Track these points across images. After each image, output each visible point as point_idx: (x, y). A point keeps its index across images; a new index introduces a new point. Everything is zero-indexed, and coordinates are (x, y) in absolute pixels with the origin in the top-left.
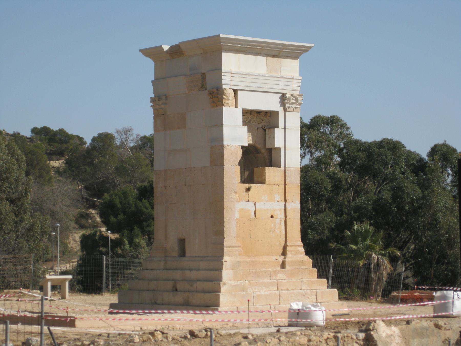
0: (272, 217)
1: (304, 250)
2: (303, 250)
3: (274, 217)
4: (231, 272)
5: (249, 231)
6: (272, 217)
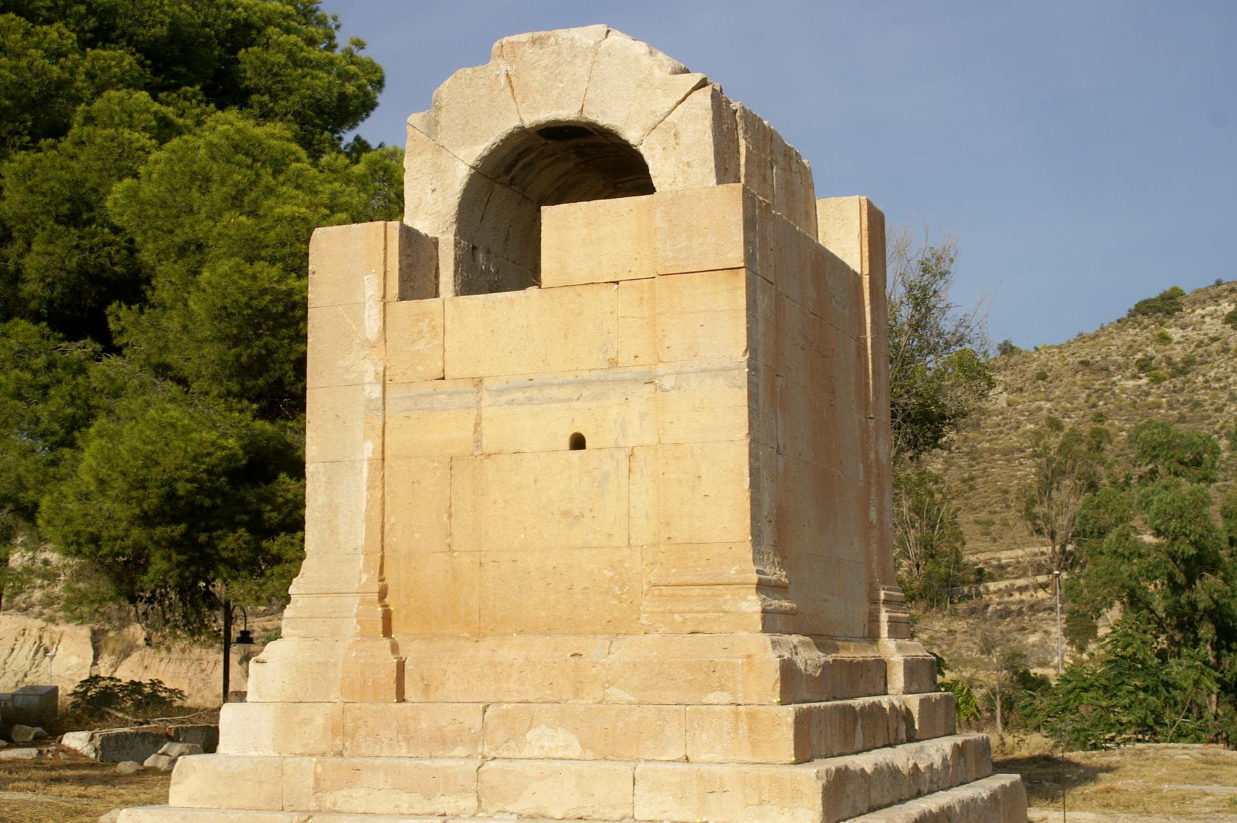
5: (445, 516)
6: (578, 442)
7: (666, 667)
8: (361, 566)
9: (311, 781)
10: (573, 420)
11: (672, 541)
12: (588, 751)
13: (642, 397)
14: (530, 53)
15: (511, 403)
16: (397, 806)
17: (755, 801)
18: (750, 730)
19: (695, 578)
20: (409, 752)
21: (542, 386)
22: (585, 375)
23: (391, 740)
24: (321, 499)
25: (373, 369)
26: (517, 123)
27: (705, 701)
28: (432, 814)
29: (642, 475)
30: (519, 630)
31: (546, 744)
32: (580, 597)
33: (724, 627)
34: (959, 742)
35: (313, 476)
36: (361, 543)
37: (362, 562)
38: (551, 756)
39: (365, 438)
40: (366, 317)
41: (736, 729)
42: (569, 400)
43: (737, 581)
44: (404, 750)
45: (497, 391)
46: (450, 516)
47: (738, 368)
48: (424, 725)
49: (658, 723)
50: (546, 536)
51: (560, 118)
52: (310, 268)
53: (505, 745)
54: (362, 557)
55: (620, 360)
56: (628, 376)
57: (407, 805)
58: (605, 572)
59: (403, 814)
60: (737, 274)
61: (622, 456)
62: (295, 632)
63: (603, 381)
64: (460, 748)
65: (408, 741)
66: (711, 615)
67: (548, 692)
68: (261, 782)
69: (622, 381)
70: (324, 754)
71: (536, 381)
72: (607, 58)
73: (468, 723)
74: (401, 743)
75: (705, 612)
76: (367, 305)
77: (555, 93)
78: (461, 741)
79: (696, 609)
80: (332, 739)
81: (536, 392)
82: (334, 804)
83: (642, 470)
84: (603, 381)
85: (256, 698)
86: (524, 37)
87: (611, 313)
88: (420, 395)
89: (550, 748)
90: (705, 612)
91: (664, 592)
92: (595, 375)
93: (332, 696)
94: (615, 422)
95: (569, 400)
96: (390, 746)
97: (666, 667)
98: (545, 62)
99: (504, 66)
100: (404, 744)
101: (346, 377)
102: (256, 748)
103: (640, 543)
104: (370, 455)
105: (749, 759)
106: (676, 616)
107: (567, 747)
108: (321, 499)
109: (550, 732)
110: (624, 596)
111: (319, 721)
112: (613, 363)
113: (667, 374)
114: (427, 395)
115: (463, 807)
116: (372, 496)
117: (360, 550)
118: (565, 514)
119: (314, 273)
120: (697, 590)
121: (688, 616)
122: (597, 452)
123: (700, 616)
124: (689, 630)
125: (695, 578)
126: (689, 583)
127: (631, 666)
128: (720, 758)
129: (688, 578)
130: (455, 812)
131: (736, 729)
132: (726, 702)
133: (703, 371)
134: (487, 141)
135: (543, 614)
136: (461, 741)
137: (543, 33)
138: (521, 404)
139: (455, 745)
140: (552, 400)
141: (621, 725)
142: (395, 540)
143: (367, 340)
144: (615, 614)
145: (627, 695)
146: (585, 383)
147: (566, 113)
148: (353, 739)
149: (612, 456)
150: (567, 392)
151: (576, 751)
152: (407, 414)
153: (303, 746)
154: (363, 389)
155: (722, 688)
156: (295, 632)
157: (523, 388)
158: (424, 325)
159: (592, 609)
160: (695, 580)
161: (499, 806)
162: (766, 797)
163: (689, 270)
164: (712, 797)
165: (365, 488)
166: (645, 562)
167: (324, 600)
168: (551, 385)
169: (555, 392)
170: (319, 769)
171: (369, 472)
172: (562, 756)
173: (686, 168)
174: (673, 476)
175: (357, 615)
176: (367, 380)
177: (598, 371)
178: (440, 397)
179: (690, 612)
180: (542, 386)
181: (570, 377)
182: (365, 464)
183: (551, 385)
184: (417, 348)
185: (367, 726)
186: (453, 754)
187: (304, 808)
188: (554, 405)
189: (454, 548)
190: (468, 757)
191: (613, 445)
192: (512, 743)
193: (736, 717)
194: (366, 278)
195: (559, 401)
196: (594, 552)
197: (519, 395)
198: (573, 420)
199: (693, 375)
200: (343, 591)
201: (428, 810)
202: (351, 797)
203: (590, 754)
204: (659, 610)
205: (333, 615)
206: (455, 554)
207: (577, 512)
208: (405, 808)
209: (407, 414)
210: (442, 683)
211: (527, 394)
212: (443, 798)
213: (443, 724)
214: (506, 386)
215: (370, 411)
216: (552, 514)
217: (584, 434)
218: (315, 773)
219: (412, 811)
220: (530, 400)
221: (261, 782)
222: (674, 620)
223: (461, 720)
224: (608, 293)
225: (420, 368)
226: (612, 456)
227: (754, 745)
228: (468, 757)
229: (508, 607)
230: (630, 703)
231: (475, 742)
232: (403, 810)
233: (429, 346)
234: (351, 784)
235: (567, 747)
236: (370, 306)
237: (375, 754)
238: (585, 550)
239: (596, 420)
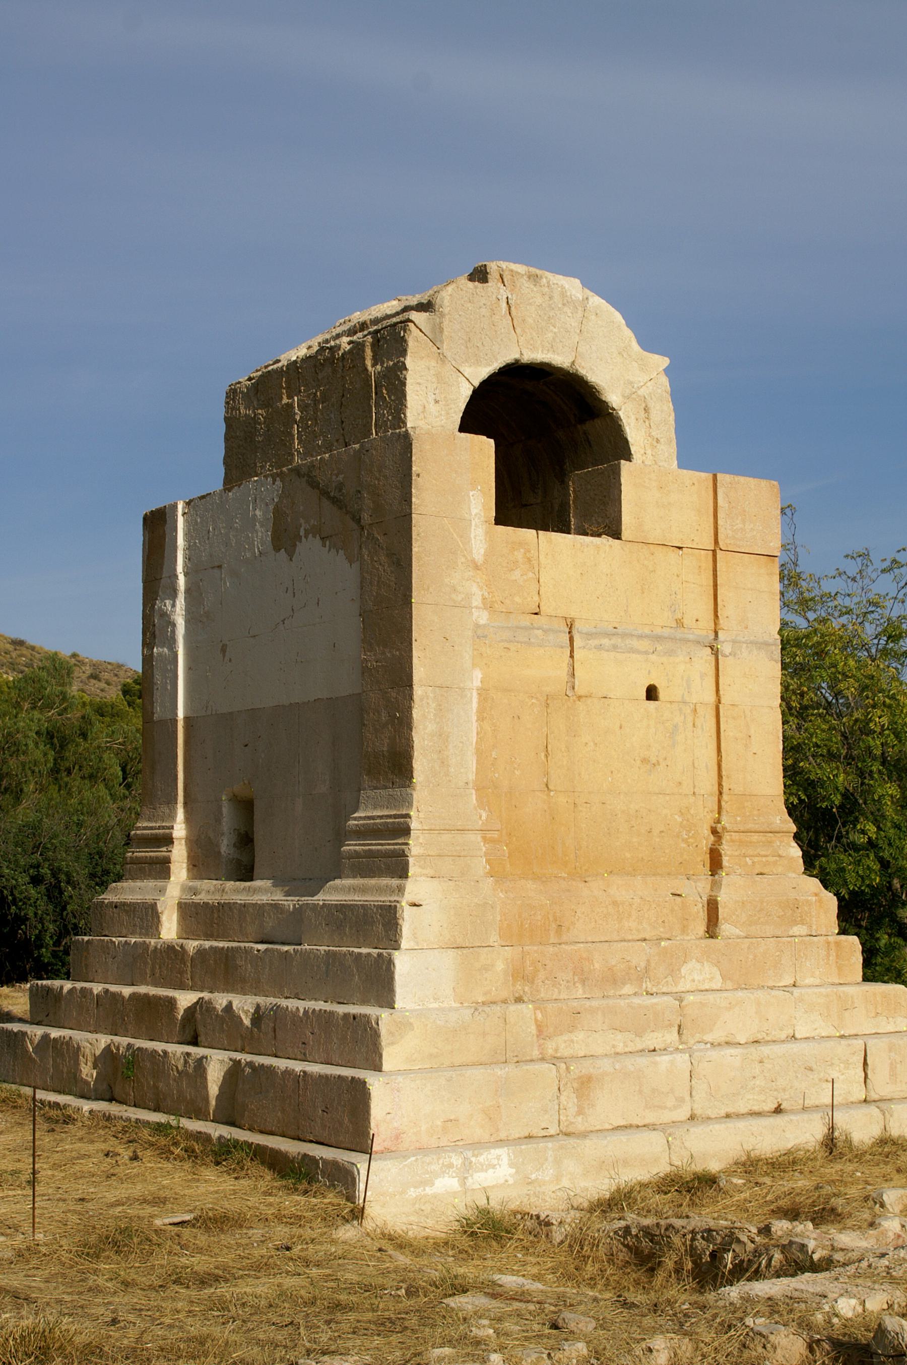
0: (652, 693)
1: (800, 853)
2: (796, 852)
3: (662, 694)
4: (447, 961)
5: (543, 755)
6: (652, 693)
7: (765, 904)
8: (475, 801)
9: (533, 1029)
10: (649, 672)
11: (732, 792)
12: (728, 982)
13: (702, 658)
14: (526, 286)
15: (599, 647)
16: (614, 1046)
17: (873, 1014)
18: (837, 956)
19: (757, 826)
20: (584, 993)
21: (624, 635)
22: (658, 631)
23: (568, 982)
24: (431, 727)
25: (480, 593)
26: (517, 356)
27: (791, 933)
28: (642, 1051)
29: (703, 729)
30: (609, 870)
31: (696, 978)
32: (658, 840)
33: (780, 869)
34: (262, 1004)
35: (422, 700)
36: (472, 777)
37: (474, 797)
38: (699, 988)
39: (474, 665)
40: (472, 536)
41: (828, 955)
42: (646, 653)
43: (785, 830)
44: (581, 991)
45: (586, 634)
46: (547, 756)
47: (775, 645)
48: (597, 966)
49: (777, 954)
50: (629, 780)
51: (554, 362)
52: (414, 469)
53: (665, 980)
54: (474, 792)
55: (685, 621)
56: (691, 637)
57: (621, 1045)
58: (676, 817)
59: (618, 1053)
60: (773, 562)
61: (688, 710)
62: (424, 871)
63: (672, 639)
64: (628, 986)
65: (583, 982)
66: (771, 859)
67: (662, 929)
68: (484, 1034)
69: (687, 641)
70: (505, 1002)
71: (619, 631)
72: (593, 317)
73: (634, 963)
74: (577, 985)
75: (767, 856)
76: (473, 523)
77: (550, 335)
78: (629, 979)
79: (763, 853)
80: (513, 985)
81: (620, 640)
82: (556, 1050)
83: (702, 725)
84: (672, 639)
85: (412, 945)
86: (520, 268)
87: (678, 576)
88: (517, 627)
89: (699, 981)
90: (767, 856)
91: (733, 837)
92: (666, 632)
93: (491, 940)
94: (682, 678)
95: (646, 653)
96: (568, 988)
97: (765, 904)
98: (539, 300)
99: (504, 293)
100: (579, 985)
101: (454, 596)
102: (436, 999)
103: (702, 792)
104: (479, 684)
105: (837, 981)
106: (748, 859)
107: (711, 979)
108: (431, 727)
109: (698, 966)
110: (691, 840)
111: (500, 966)
112: (680, 623)
113: (727, 641)
114: (525, 628)
115: (669, 1041)
116: (482, 728)
117: (471, 785)
118: (645, 761)
119: (418, 475)
120: (755, 837)
121: (756, 859)
122: (669, 705)
123: (764, 859)
124: (757, 872)
125: (757, 826)
126: (753, 830)
127: (741, 904)
128: (817, 982)
129: (750, 826)
130: (662, 1046)
131: (828, 955)
132: (805, 933)
133: (751, 643)
134: (490, 365)
135: (628, 855)
136: (629, 979)
137: (539, 272)
138: (608, 651)
139: (624, 984)
140: (633, 650)
141: (751, 957)
142: (497, 775)
143: (473, 561)
144: (685, 857)
145: (737, 931)
146: (659, 638)
147: (560, 359)
148: (532, 983)
149: (680, 710)
150: (644, 645)
151: (717, 983)
152: (506, 645)
153: (485, 994)
154: (471, 613)
155: (802, 923)
156: (424, 871)
157: (607, 635)
158: (519, 555)
159: (667, 851)
160: (756, 827)
161: (698, 1037)
162: (879, 1010)
163: (743, 551)
164: (847, 1014)
165: (474, 718)
166: (706, 810)
167: (446, 837)
168: (632, 635)
169: (635, 643)
170: (539, 1016)
171: (479, 702)
172: (707, 987)
173: (655, 444)
174: (731, 734)
175: (486, 854)
176: (475, 604)
177: (668, 629)
178: (536, 632)
179: (759, 855)
180: (624, 635)
181: (647, 631)
182: (475, 694)
183: (632, 635)
184: (514, 578)
185: (545, 969)
186: (623, 992)
187: (528, 1058)
188: (634, 655)
189: (550, 787)
190: (635, 994)
191: (680, 699)
192: (670, 979)
193: (828, 946)
194: (471, 493)
195: (638, 652)
196: (668, 798)
197: (606, 642)
198: (649, 672)
199: (745, 645)
200: (467, 828)
201: (640, 1047)
202: (572, 1041)
203: (729, 985)
204: (736, 853)
205: (462, 854)
206: (552, 794)
207: (654, 760)
208: (620, 1048)
209: (506, 645)
210: (573, 923)
211: (612, 642)
212: (652, 1033)
213: (613, 963)
214: (594, 630)
215: (478, 637)
216: (635, 760)
217: (657, 685)
218: (536, 1020)
219: (627, 1050)
220: (615, 647)
221: (484, 1034)
222: (746, 863)
223: (629, 958)
224: (674, 555)
225: (517, 599)
226: (680, 710)
227: (840, 968)
228: (635, 994)
229: (600, 848)
230: (738, 937)
231: (640, 980)
232: (619, 1050)
233: (525, 577)
234: (572, 1028)
235: (711, 979)
236: (476, 525)
237: (554, 997)
238: (661, 796)
239: (667, 675)
